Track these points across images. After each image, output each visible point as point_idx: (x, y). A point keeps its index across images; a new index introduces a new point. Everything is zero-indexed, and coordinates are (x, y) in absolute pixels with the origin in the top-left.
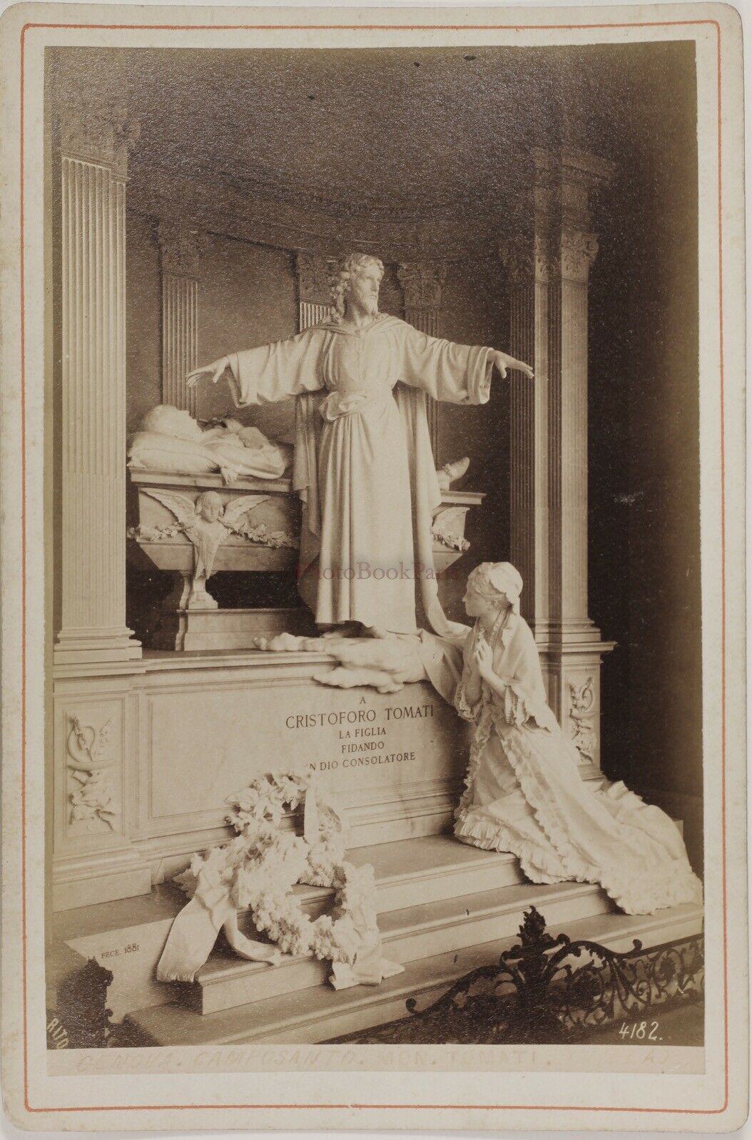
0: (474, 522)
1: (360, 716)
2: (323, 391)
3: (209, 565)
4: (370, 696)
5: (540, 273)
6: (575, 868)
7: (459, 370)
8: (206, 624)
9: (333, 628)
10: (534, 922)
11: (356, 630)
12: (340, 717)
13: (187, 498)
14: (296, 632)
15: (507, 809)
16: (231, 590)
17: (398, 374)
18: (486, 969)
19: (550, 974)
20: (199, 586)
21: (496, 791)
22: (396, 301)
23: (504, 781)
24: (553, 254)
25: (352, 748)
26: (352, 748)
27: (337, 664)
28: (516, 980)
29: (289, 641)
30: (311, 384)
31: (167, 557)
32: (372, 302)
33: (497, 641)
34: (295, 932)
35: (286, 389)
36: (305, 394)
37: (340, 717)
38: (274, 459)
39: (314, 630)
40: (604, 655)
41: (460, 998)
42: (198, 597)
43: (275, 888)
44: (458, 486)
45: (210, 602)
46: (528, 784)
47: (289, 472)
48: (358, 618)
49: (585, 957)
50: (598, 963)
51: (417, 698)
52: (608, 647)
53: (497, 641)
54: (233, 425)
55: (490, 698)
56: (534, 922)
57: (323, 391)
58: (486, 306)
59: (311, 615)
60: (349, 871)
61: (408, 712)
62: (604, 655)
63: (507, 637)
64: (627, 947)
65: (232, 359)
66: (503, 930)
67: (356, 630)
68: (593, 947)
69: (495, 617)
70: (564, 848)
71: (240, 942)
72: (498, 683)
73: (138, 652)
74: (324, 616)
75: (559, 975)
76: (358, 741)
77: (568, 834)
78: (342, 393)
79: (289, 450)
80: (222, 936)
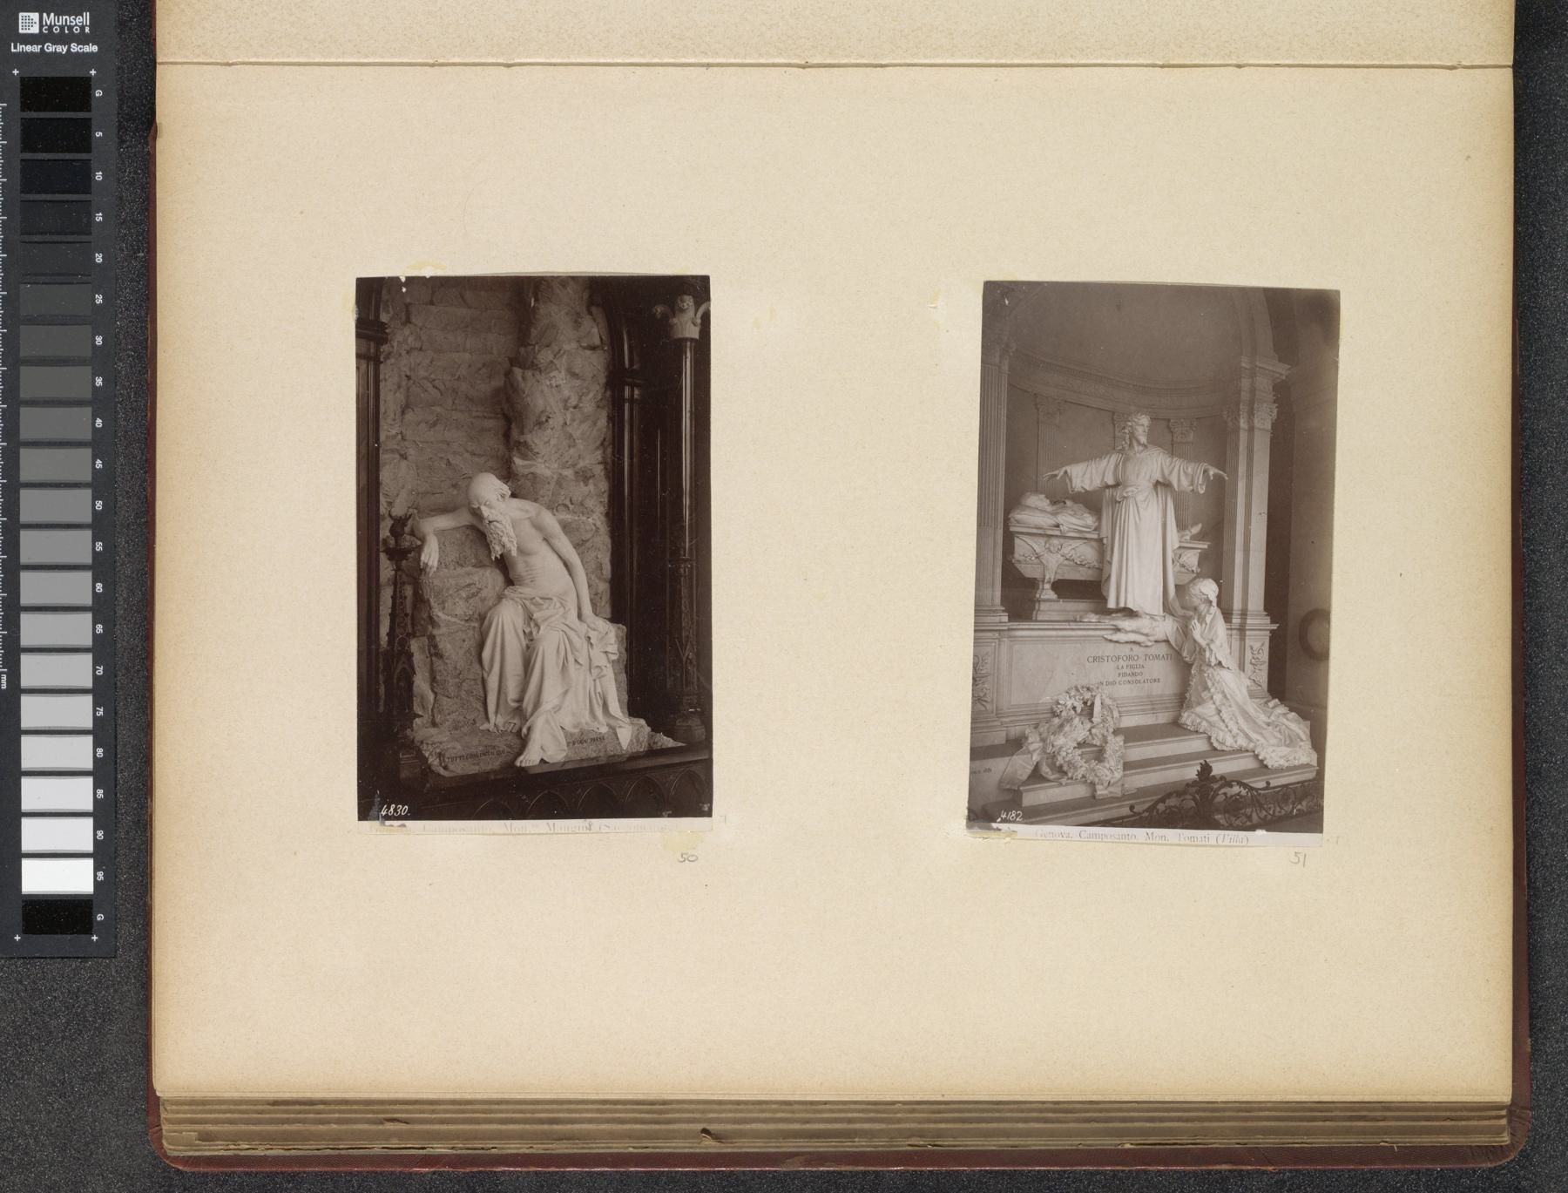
0: (1203, 558)
1: (1130, 658)
2: (1117, 485)
3: (1051, 576)
4: (1136, 648)
5: (1243, 424)
6: (1242, 742)
7: (1189, 475)
8: (1049, 603)
9: (1118, 610)
10: (1206, 769)
11: (1130, 613)
12: (1118, 658)
13: (1042, 541)
14: (1096, 612)
15: (1207, 710)
16: (1065, 588)
17: (1157, 476)
18: (1181, 790)
19: (1214, 797)
20: (1047, 586)
21: (1200, 702)
22: (1154, 441)
23: (1205, 695)
24: (1251, 414)
25: (1125, 675)
26: (1125, 675)
27: (1118, 630)
28: (1194, 799)
29: (1093, 618)
30: (1111, 482)
31: (1029, 571)
32: (1143, 440)
33: (1202, 619)
34: (1076, 768)
35: (1097, 483)
36: (1108, 487)
37: (1118, 658)
38: (1089, 520)
39: (1109, 612)
40: (1272, 631)
41: (1161, 807)
42: (1047, 593)
43: (1066, 743)
44: (1194, 538)
45: (1052, 595)
46: (1218, 697)
47: (1097, 529)
48: (1130, 605)
49: (1236, 789)
50: (1244, 792)
51: (1162, 650)
52: (1275, 627)
53: (1202, 619)
54: (1069, 503)
55: (1199, 651)
56: (1206, 769)
57: (1117, 485)
58: (1218, 443)
59: (1105, 600)
60: (1110, 738)
61: (1157, 657)
62: (1272, 631)
63: (1208, 619)
64: (1262, 785)
65: (1068, 469)
66: (1191, 773)
67: (1130, 613)
68: (1245, 786)
69: (1203, 607)
70: (1235, 731)
71: (1045, 769)
72: (1203, 643)
73: (1006, 619)
74: (1111, 604)
75: (1220, 798)
76: (1128, 671)
77: (1239, 721)
78: (1125, 487)
79: (1099, 519)
80: (1037, 767)
